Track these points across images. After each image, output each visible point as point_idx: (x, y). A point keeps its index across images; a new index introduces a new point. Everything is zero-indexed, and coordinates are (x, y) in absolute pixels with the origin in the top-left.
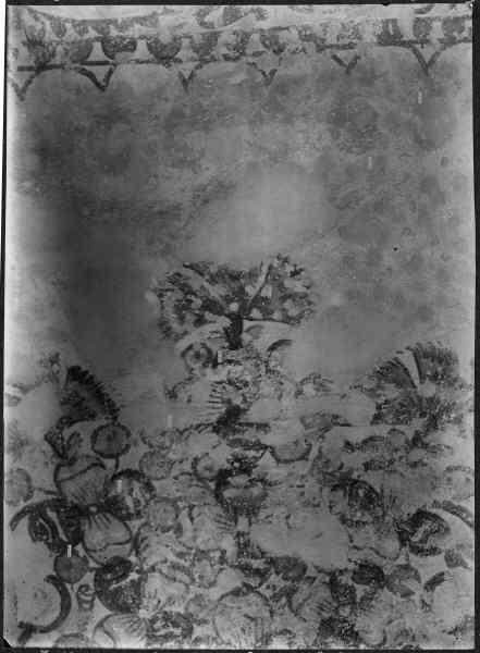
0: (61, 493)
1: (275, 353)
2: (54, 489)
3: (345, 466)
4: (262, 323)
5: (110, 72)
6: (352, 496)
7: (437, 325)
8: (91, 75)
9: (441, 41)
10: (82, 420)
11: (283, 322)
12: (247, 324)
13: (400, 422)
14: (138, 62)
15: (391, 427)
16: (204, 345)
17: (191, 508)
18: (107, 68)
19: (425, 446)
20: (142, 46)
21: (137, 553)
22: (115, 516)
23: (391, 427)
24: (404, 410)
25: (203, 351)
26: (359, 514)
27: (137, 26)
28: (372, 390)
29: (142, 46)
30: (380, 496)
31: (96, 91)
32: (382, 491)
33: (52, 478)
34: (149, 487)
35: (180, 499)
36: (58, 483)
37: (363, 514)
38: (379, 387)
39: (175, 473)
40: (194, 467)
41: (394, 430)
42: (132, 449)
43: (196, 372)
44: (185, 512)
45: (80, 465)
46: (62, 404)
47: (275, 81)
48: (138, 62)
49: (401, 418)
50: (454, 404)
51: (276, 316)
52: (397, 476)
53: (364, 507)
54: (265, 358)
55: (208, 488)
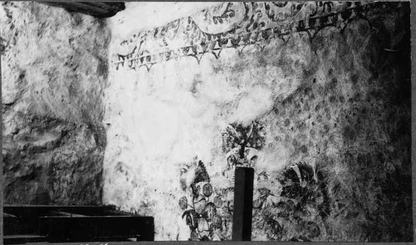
0: (194, 208)
1: (253, 161)
2: (192, 206)
3: (108, 183)
4: (250, 148)
5: (220, 52)
6: (273, 227)
7: (315, 132)
8: (214, 53)
9: (318, 27)
10: (201, 181)
11: (256, 148)
12: (246, 148)
13: (292, 197)
14: (228, 47)
15: (289, 199)
16: (234, 156)
17: (226, 221)
18: (218, 51)
19: (301, 210)
20: (229, 41)
21: (211, 236)
22: (206, 219)
23: (289, 199)
24: (278, 230)
25: (233, 158)
26: (273, 235)
27: (229, 34)
28: (282, 181)
29: (229, 41)
30: (282, 229)
31: (215, 59)
32: (283, 226)
33: (105, 190)
34: (215, 210)
35: (223, 217)
36: (194, 203)
37: (275, 236)
38: (285, 180)
39: (223, 206)
40: (228, 205)
41: (290, 200)
42: (212, 195)
43: (231, 166)
44: (223, 223)
45: (200, 198)
46: (196, 174)
47: (264, 50)
48: (228, 47)
49: (293, 195)
50: (312, 192)
51: (254, 146)
52: (289, 221)
53: (276, 233)
54: (249, 163)
55: (231, 214)
